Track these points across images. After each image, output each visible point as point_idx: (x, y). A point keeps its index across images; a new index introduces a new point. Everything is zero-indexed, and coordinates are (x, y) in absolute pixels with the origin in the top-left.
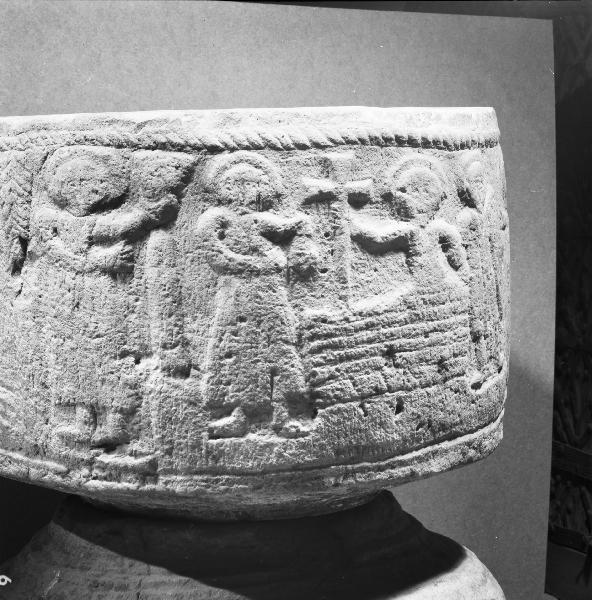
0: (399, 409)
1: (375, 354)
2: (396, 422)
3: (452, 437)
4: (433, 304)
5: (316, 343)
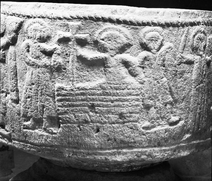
0: (98, 131)
1: (85, 106)
2: (96, 136)
3: (131, 147)
4: (117, 89)
5: (60, 97)
